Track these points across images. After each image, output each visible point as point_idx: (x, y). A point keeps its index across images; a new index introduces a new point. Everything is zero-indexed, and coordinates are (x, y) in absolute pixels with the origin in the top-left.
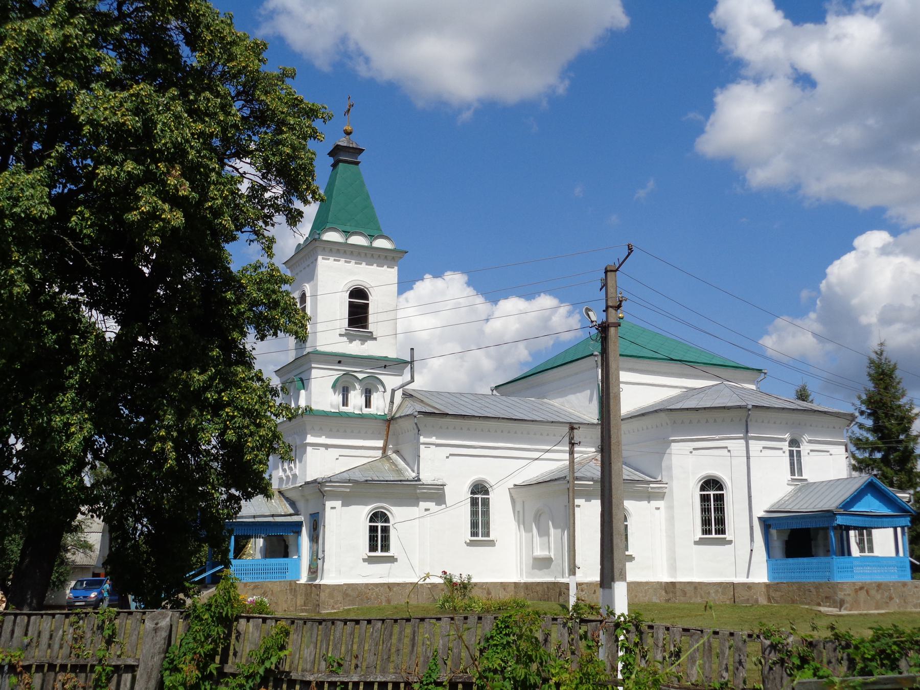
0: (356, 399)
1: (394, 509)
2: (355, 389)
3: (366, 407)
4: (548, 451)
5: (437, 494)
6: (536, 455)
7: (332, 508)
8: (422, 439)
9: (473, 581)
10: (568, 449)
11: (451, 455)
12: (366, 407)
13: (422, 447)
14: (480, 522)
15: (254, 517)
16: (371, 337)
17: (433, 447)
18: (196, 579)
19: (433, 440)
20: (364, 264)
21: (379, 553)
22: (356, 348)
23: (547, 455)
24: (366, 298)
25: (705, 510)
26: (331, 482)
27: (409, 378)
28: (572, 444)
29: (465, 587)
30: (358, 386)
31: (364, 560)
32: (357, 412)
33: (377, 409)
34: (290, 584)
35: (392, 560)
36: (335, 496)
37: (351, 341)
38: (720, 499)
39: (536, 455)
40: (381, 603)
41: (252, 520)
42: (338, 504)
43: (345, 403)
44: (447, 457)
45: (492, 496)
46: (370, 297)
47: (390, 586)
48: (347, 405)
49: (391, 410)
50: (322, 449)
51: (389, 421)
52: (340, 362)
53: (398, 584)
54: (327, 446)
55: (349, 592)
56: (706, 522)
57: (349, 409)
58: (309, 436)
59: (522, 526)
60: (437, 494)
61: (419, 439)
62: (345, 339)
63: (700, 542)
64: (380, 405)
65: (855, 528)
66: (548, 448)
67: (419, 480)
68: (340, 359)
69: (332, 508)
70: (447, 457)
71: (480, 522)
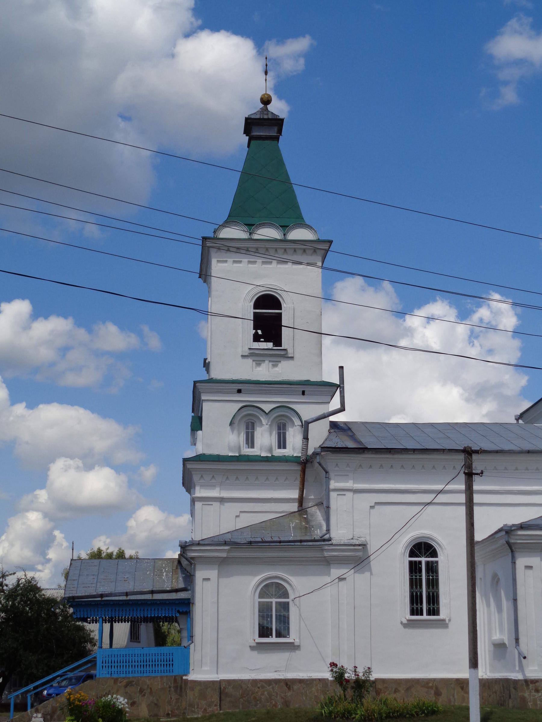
0: (265, 440)
1: (293, 579)
2: (262, 425)
3: (279, 447)
4: (441, 492)
5: (357, 557)
6: (428, 498)
7: (205, 579)
8: (333, 484)
9: (374, 676)
10: (463, 487)
11: (377, 504)
12: (279, 447)
13: (333, 495)
14: (424, 597)
15: (127, 594)
16: (286, 356)
17: (350, 495)
18: (90, 665)
19: (349, 484)
20: (274, 262)
21: (273, 639)
22: (264, 372)
23: (442, 498)
24: (279, 307)
25: (415, 583)
26: (199, 544)
27: (339, 406)
28: (470, 475)
29: (361, 686)
30: (264, 421)
31: (252, 648)
32: (264, 454)
33: (294, 449)
34: (175, 680)
35: (293, 647)
36: (209, 561)
37: (259, 364)
38: (432, 569)
39: (428, 498)
40: (275, 705)
41: (124, 598)
42: (212, 573)
43: (250, 442)
44: (372, 507)
45: (441, 559)
46: (284, 305)
47: (288, 684)
48: (285, 447)
49: (305, 447)
50: (216, 505)
51: (305, 463)
52: (239, 391)
53: (301, 681)
54: (222, 500)
55: (230, 690)
56: (415, 600)
57: (255, 451)
58: (197, 488)
59: (484, 599)
60: (357, 557)
61: (328, 484)
62: (249, 361)
63: (409, 624)
64: (294, 445)
65: (146, 620)
66: (440, 487)
67: (330, 540)
68: (240, 386)
69: (205, 579)
70: (372, 507)
71: (424, 597)
